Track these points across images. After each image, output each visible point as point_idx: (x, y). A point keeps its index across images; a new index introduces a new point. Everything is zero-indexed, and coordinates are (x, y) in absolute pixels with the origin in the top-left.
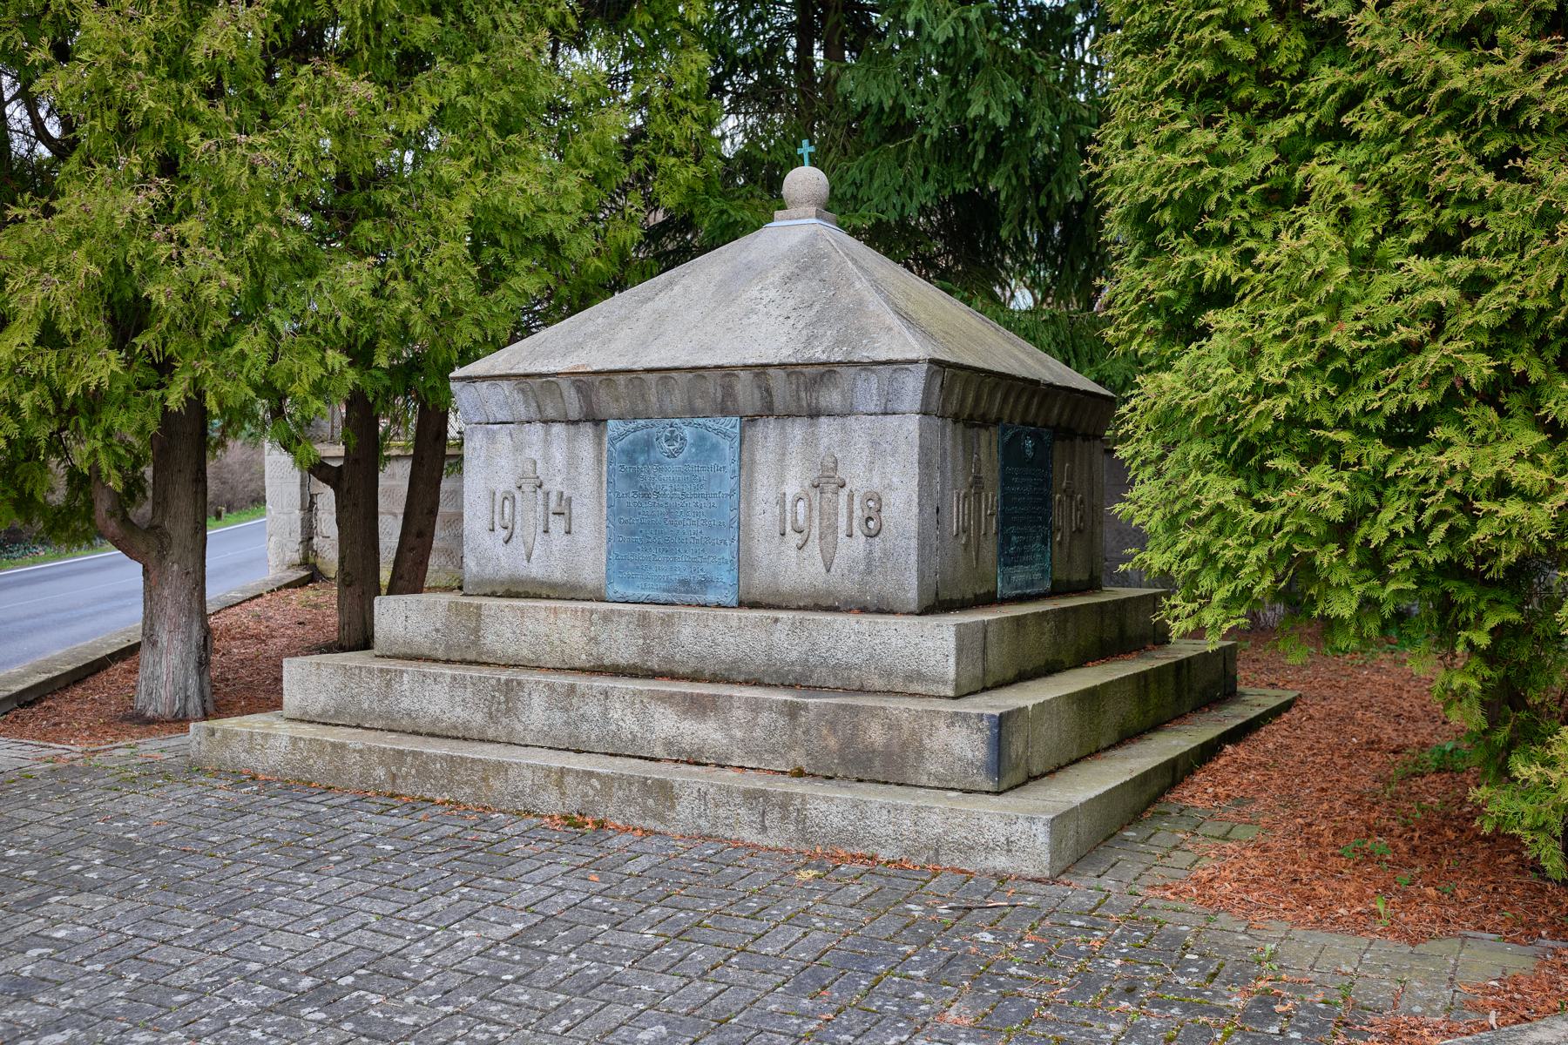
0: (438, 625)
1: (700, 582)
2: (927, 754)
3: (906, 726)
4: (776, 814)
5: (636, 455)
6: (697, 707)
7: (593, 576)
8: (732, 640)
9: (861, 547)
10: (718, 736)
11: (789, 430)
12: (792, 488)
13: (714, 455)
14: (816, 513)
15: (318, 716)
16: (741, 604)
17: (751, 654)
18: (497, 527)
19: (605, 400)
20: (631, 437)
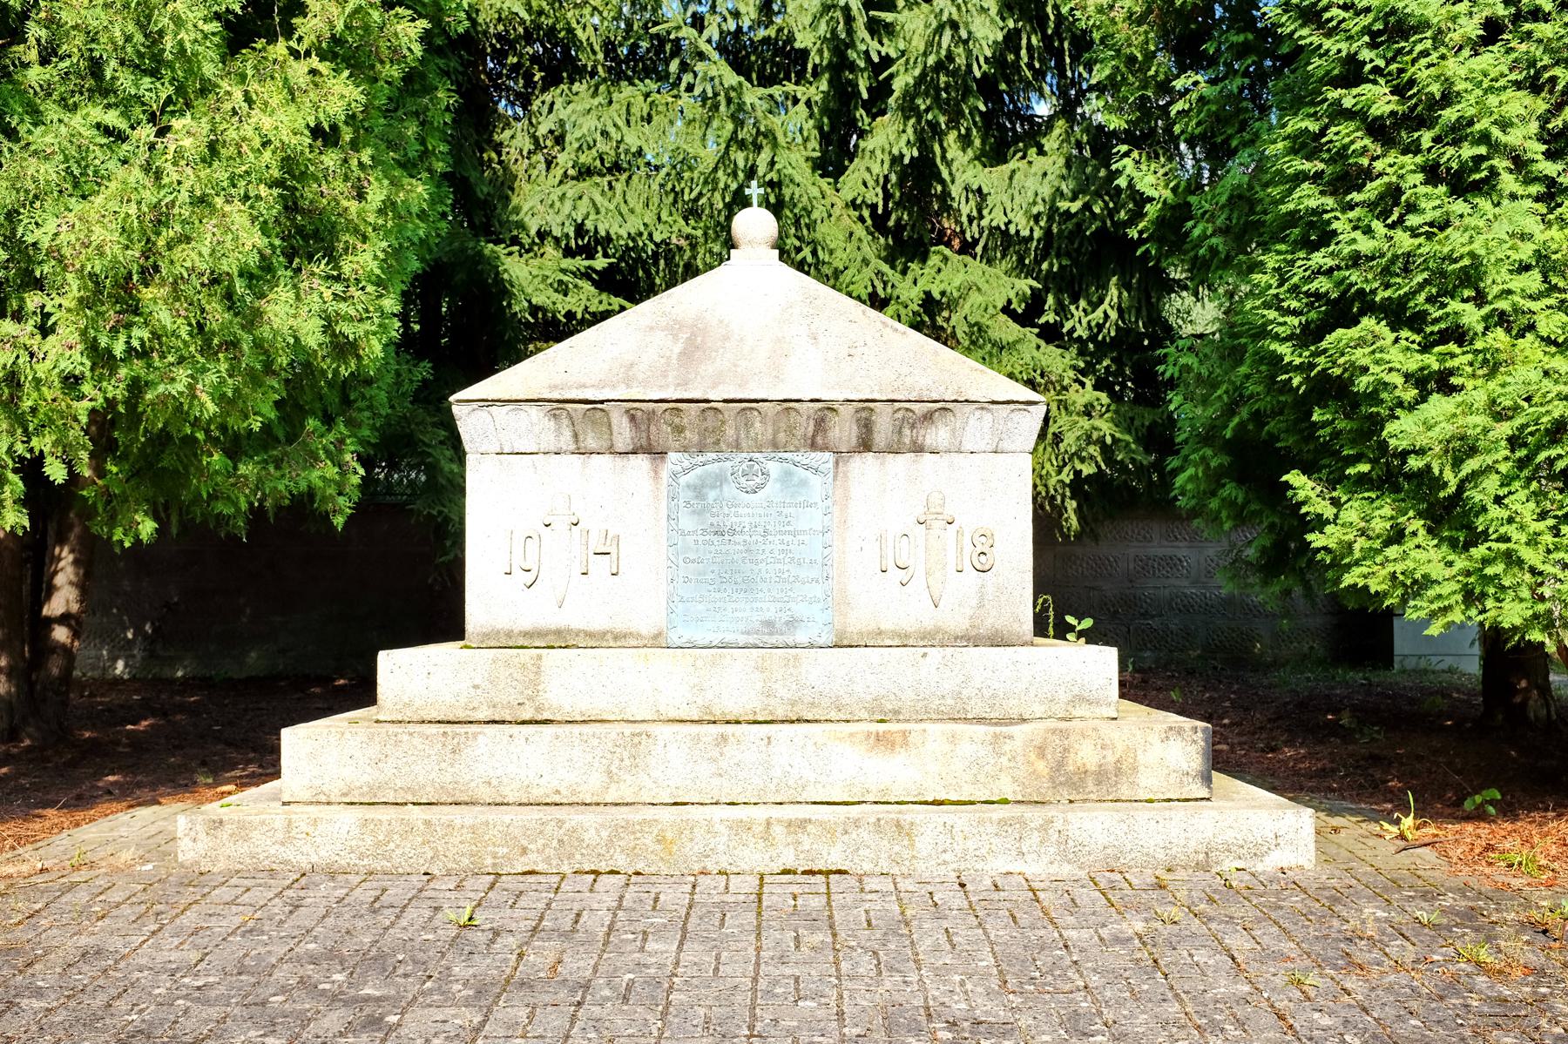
1: (787, 623)
19: (662, 433)
20: (699, 471)
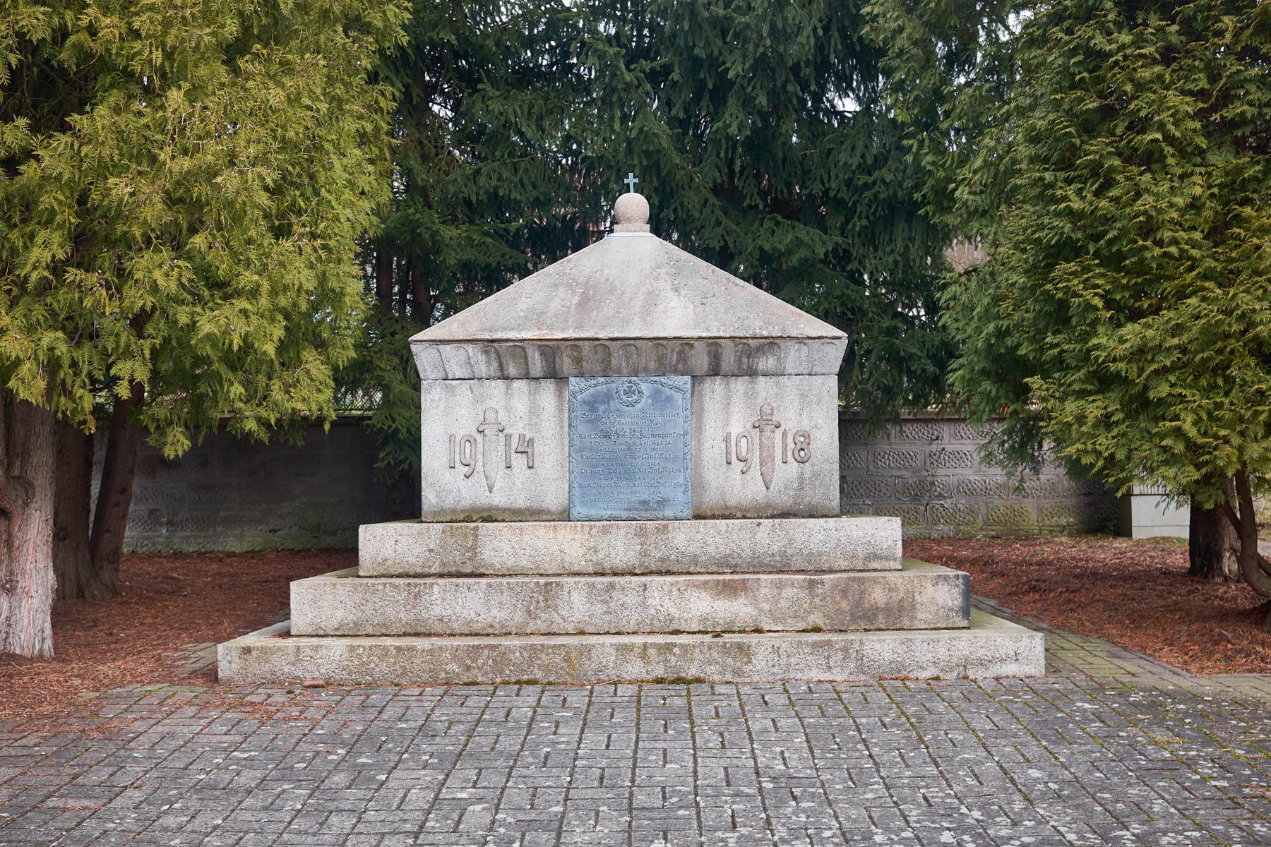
0: (432, 546)
1: (658, 502)
2: (918, 606)
3: (901, 588)
4: (840, 655)
5: (596, 405)
6: (729, 590)
7: (556, 502)
8: (721, 541)
9: (795, 470)
10: (749, 609)
11: (732, 386)
12: (736, 429)
13: (669, 405)
14: (757, 447)
15: (337, 629)
16: (697, 517)
17: (738, 551)
18: (458, 465)
